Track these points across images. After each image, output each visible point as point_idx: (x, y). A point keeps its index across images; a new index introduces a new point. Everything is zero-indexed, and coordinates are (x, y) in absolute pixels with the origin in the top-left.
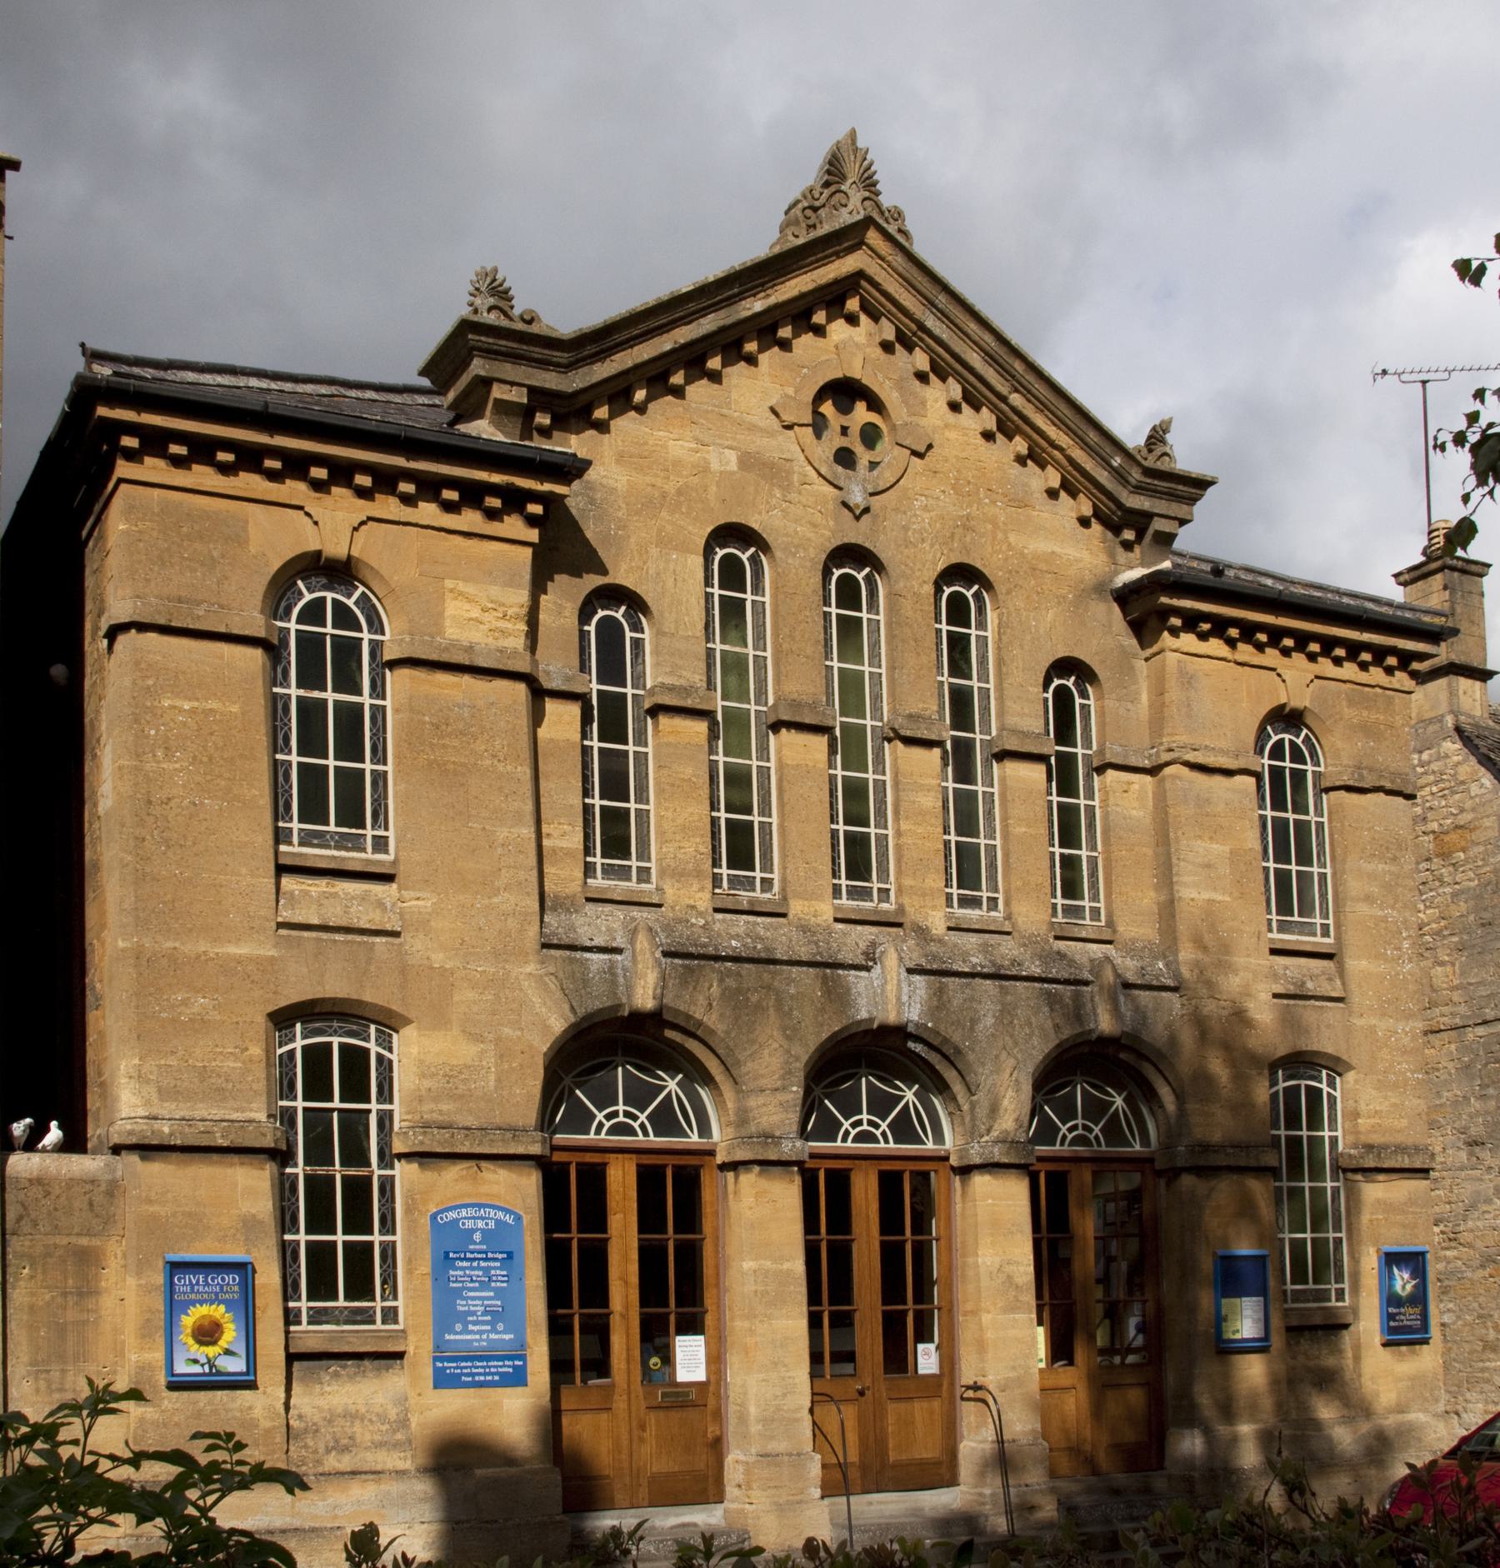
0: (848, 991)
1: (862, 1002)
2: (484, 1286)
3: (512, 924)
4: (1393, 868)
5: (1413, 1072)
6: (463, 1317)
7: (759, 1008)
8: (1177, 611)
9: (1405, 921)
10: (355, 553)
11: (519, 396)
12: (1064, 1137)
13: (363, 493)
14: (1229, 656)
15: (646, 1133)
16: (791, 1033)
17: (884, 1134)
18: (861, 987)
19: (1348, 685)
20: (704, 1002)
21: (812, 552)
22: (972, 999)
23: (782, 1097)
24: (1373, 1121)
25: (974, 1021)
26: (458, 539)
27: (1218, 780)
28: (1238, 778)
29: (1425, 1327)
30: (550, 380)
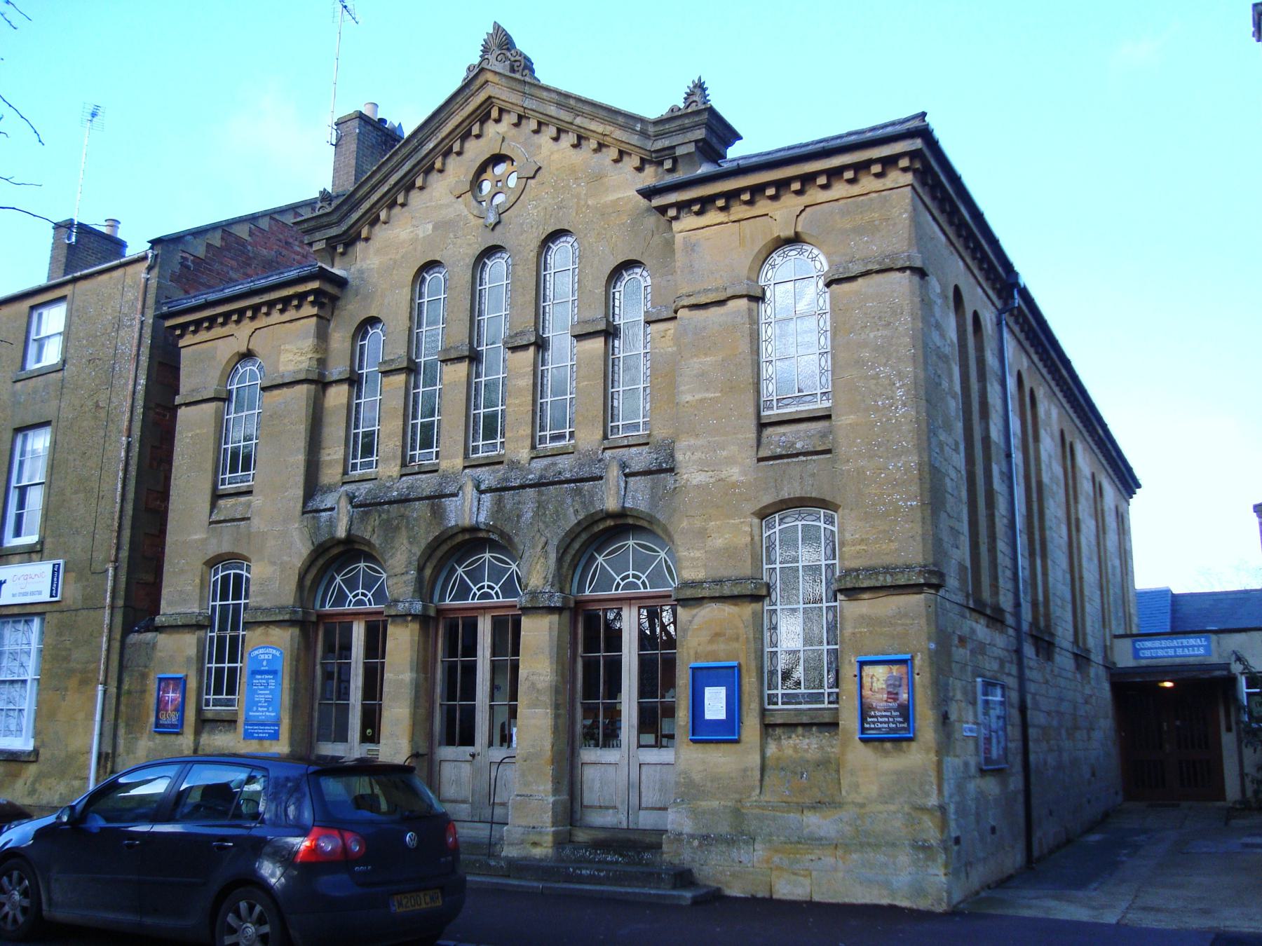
0: (445, 511)
1: (452, 515)
2: (266, 688)
3: (292, 504)
4: (885, 332)
5: (906, 501)
6: (256, 704)
7: (398, 528)
8: (174, 327)
9: (899, 373)
10: (799, 229)
11: (322, 245)
12: (618, 584)
13: (799, 193)
14: (726, 220)
15: (645, 587)
16: (412, 540)
17: (497, 593)
18: (453, 508)
19: (842, 202)
20: (370, 532)
21: (467, 260)
22: (519, 503)
23: (405, 578)
24: (858, 547)
25: (519, 517)
26: (287, 325)
27: (714, 310)
28: (731, 304)
29: (182, 725)
30: (334, 232)
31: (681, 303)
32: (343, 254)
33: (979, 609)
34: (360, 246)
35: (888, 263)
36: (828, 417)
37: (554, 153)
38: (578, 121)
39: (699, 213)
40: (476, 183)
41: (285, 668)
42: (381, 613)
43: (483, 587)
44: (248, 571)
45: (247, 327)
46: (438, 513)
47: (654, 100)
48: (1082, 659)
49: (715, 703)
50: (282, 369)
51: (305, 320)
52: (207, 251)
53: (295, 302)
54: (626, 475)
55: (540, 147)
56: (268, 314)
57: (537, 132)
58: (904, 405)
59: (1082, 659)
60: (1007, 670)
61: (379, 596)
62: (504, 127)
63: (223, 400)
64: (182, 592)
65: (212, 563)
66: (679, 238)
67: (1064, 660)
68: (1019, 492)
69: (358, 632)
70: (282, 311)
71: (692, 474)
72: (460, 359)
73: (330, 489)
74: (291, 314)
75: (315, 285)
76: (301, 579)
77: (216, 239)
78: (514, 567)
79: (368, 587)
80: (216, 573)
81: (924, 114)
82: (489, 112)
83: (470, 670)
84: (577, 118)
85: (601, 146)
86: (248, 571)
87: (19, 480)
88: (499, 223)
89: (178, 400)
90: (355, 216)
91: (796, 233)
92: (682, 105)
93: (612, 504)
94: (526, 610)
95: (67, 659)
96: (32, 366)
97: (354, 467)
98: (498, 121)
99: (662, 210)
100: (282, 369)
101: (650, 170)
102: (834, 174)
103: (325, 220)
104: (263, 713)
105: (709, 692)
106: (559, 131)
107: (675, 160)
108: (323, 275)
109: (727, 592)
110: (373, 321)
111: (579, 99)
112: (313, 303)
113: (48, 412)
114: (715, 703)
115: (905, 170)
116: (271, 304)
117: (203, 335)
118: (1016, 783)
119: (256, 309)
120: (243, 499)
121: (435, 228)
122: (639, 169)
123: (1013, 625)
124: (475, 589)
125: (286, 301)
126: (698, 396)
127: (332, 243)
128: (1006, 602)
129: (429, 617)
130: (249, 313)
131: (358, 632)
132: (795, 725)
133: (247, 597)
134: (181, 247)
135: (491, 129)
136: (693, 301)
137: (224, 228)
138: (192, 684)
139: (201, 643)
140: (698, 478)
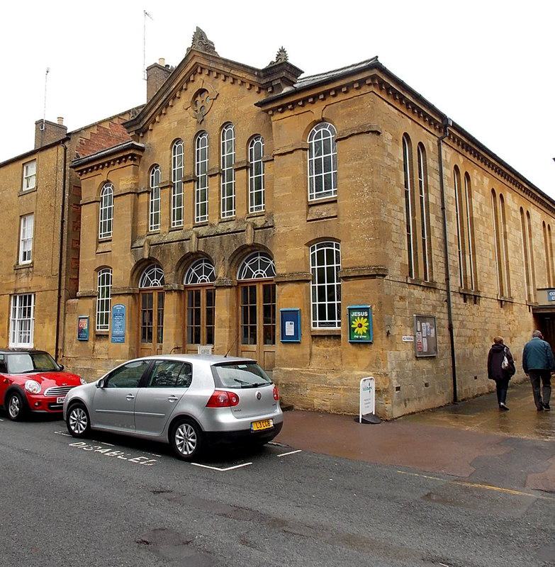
13: (323, 100)
30: (138, 127)
31: (276, 153)
32: (142, 137)
33: (416, 284)
34: (149, 132)
35: (361, 130)
36: (336, 201)
37: (223, 88)
38: (232, 72)
39: (282, 112)
40: (194, 101)
41: (126, 312)
42: (272, 281)
43: (258, 272)
44: (337, 246)
45: (106, 170)
46: (182, 248)
47: (261, 60)
48: (504, 303)
49: (290, 329)
50: (121, 188)
51: (129, 167)
52: (91, 136)
53: (124, 159)
54: (198, 238)
55: (218, 84)
56: (114, 165)
57: (216, 78)
58: (368, 194)
59: (504, 303)
60: (438, 310)
61: (213, 278)
62: (203, 76)
63: (99, 202)
64: (88, 281)
65: (98, 270)
66: (274, 124)
67: (488, 304)
68: (452, 227)
69: (155, 296)
70: (119, 163)
71: (280, 229)
72: (190, 181)
73: (142, 238)
74: (123, 164)
75: (131, 152)
76: (132, 275)
77: (95, 130)
78: (271, 262)
79: (158, 278)
80: (313, 249)
81: (377, 57)
82: (197, 69)
83: (254, 309)
84: (233, 71)
85: (243, 82)
86: (337, 246)
87: (24, 237)
88: (203, 120)
89: (81, 202)
90: (146, 120)
91: (323, 118)
92: (275, 61)
93: (249, 242)
94: (217, 287)
95: (44, 311)
96: (25, 189)
97: (224, 215)
98: (201, 73)
99: (267, 111)
100: (121, 188)
101: (263, 92)
102: (338, 90)
103: (135, 122)
104: (117, 332)
105: (287, 323)
106: (225, 76)
107: (273, 88)
108: (133, 147)
109: (294, 279)
110: (156, 166)
111: (231, 62)
112: (131, 160)
113: (33, 209)
114: (290, 329)
115: (369, 85)
116: (114, 161)
117: (89, 175)
118: (445, 362)
119: (109, 163)
120: (108, 243)
121: (178, 124)
122: (259, 92)
123: (445, 289)
124: (254, 273)
125: (120, 159)
126: (282, 195)
127: (138, 132)
128: (439, 278)
129: (182, 291)
130: (106, 165)
131: (155, 296)
132: (325, 336)
133: (338, 262)
134: (79, 135)
135: (199, 78)
136: (279, 152)
137: (98, 125)
138: (92, 320)
139: (95, 302)
140: (283, 230)
